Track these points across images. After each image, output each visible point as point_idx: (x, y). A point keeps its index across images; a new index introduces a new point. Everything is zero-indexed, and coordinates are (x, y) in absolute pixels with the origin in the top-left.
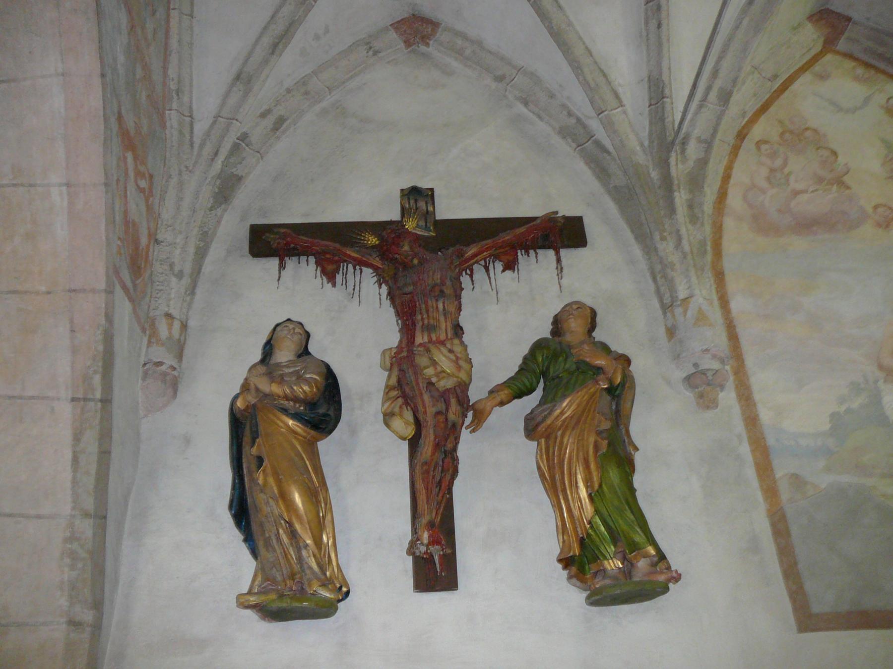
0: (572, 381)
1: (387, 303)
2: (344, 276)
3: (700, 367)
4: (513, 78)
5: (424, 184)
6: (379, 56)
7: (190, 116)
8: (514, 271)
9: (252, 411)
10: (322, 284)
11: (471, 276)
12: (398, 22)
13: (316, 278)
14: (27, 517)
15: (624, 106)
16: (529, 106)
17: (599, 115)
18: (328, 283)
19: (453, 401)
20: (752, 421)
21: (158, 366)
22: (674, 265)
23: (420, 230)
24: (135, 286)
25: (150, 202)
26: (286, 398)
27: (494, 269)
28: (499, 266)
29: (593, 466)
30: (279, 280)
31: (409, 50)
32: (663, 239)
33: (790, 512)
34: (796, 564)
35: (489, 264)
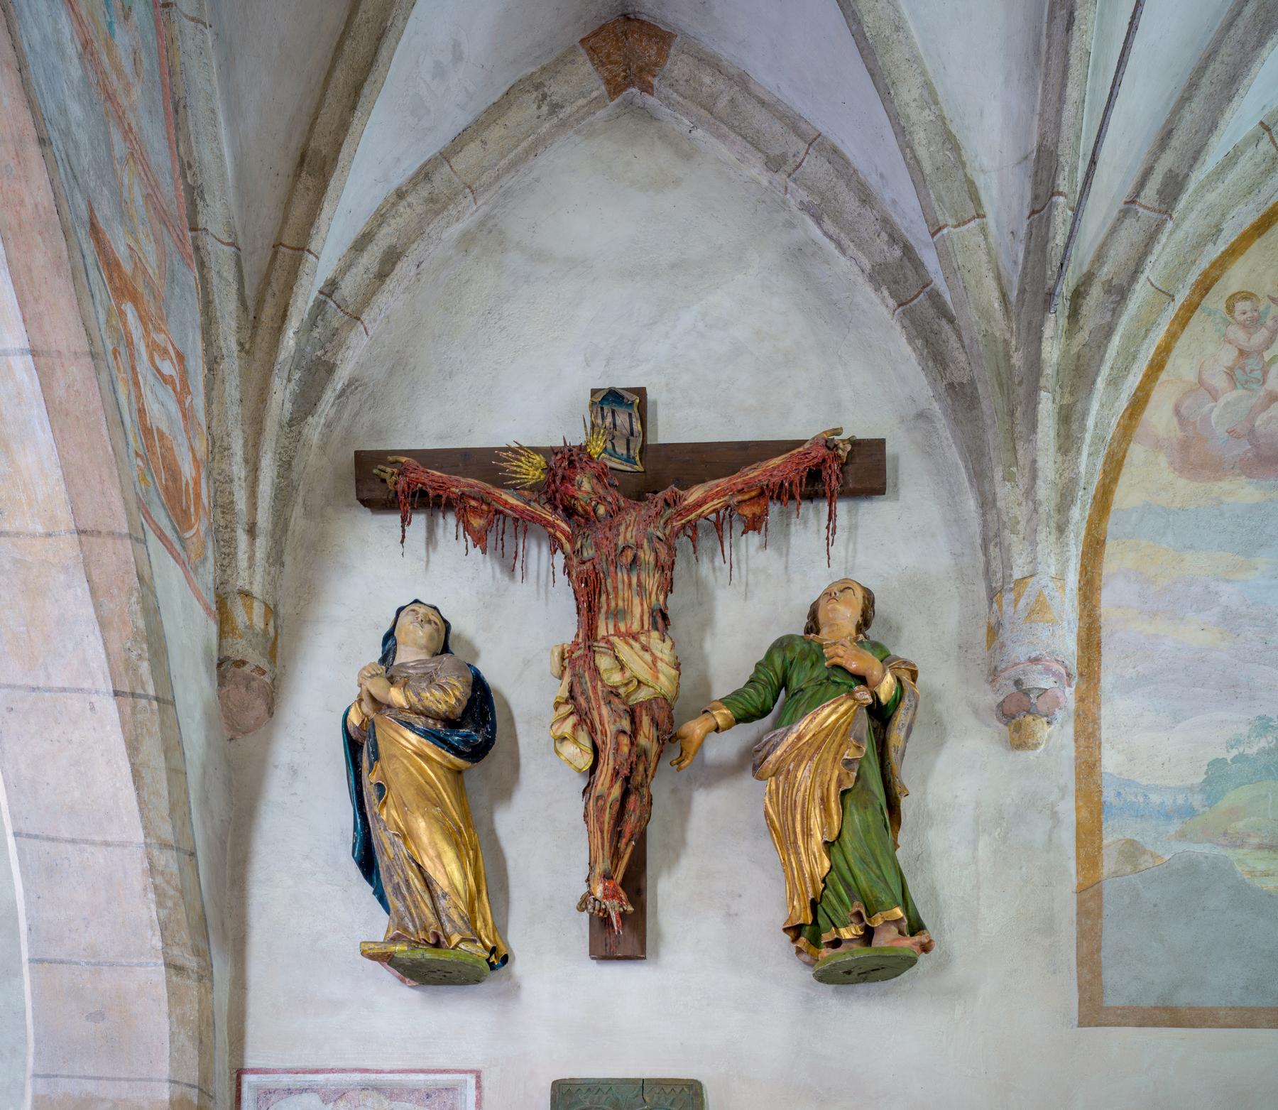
0: (819, 695)
1: (562, 578)
2: (500, 537)
3: (1025, 685)
5: (623, 381)
7: (232, 244)
8: (759, 533)
9: (368, 727)
10: (467, 548)
11: (693, 539)
14: (93, 843)
15: (984, 216)
17: (933, 235)
18: (475, 546)
19: (646, 721)
20: (1088, 768)
21: (239, 666)
22: (1018, 523)
23: (618, 461)
24: (182, 541)
25: (187, 405)
26: (412, 709)
27: (731, 528)
28: (738, 527)
30: (402, 542)
31: (617, 101)
32: (1009, 477)
33: (1108, 888)
34: (1099, 950)
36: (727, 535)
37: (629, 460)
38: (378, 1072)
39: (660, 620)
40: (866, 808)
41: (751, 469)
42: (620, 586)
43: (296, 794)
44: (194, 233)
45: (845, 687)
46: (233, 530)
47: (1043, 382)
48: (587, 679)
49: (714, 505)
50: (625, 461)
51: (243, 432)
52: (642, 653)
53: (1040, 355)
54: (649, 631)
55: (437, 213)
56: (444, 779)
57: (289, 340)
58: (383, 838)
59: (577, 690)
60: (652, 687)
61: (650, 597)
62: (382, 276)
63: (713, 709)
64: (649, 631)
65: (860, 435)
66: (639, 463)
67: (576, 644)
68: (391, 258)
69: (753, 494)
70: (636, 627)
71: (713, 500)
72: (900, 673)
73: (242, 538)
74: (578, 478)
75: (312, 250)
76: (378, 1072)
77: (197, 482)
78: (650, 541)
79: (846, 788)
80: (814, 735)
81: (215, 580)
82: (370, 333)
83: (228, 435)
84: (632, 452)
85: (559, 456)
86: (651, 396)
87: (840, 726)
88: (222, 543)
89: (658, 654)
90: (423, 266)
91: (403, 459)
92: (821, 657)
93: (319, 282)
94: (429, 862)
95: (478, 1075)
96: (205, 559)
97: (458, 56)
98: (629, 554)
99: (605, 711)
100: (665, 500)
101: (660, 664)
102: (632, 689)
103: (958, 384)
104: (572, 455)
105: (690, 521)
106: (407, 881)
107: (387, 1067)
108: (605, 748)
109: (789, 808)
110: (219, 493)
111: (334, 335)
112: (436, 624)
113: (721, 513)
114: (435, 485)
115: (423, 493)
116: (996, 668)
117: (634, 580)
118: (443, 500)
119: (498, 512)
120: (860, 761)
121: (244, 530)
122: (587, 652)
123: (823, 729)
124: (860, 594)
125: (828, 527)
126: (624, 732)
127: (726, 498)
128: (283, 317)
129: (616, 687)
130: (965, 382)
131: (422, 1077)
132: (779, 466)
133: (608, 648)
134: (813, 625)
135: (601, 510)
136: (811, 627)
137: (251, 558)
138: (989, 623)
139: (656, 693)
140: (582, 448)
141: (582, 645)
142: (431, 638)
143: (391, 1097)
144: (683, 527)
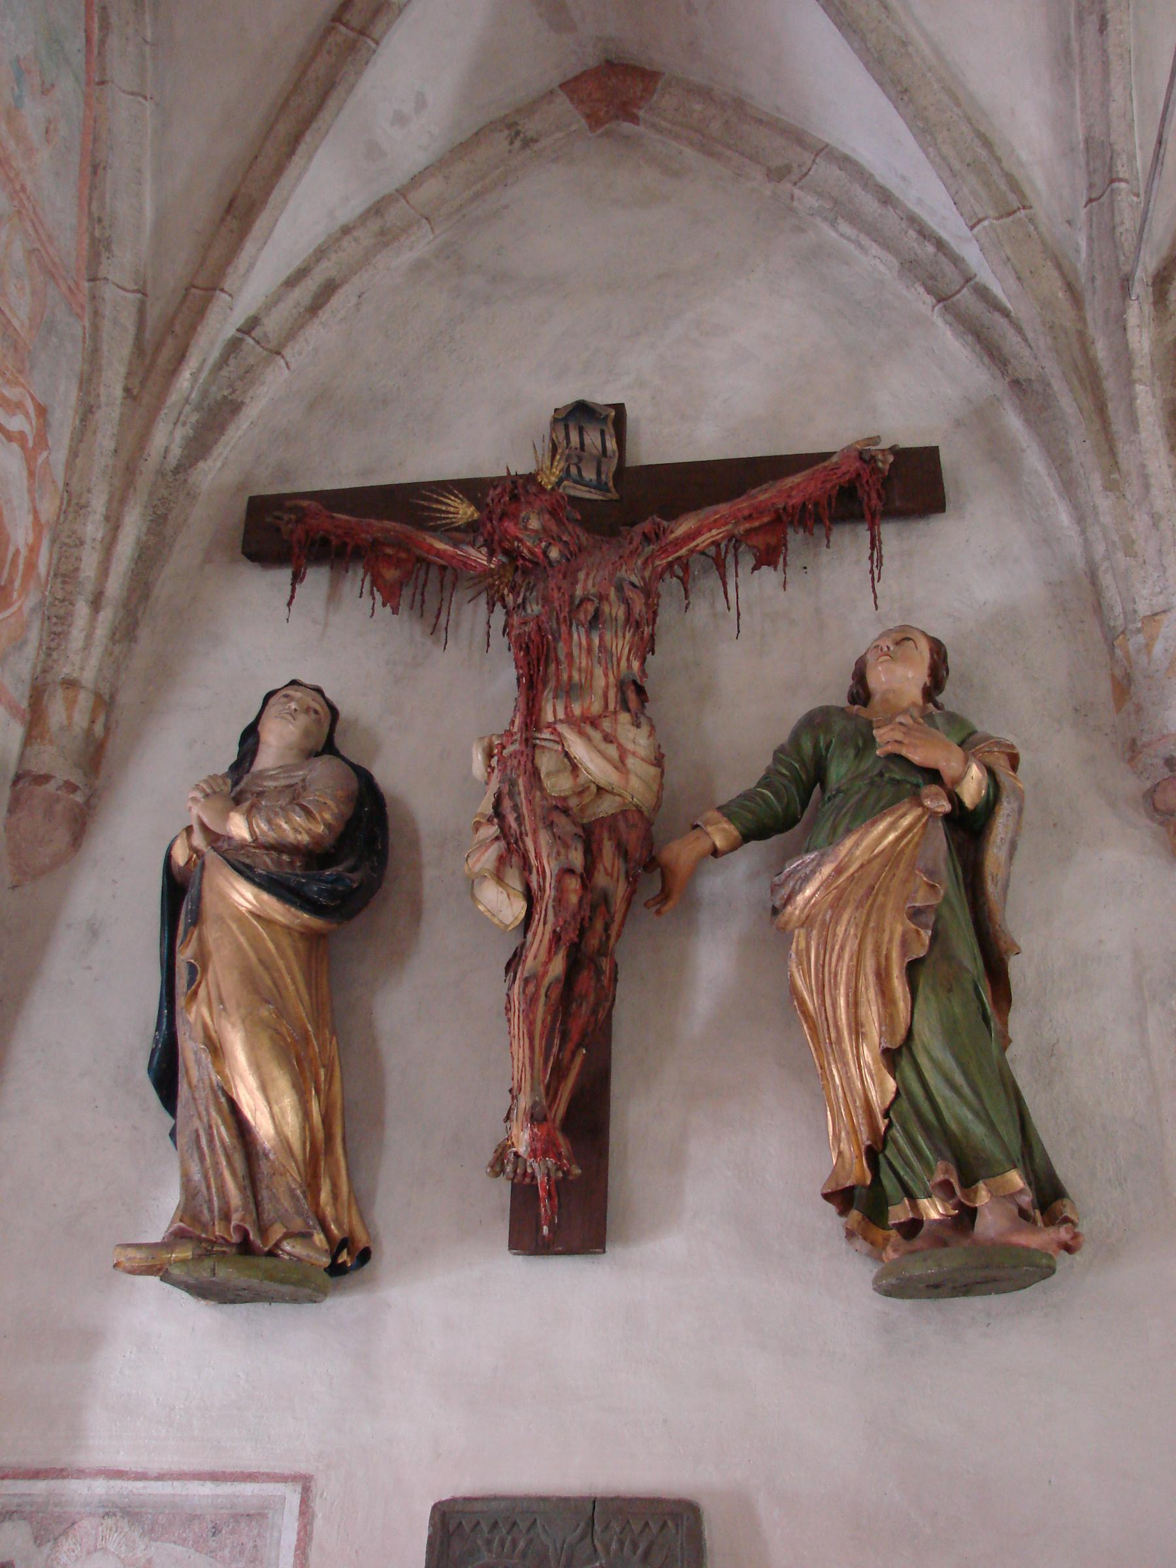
1: (500, 642)
4: (805, 170)
5: (602, 397)
6: (535, 148)
7: (138, 291)
8: (775, 569)
10: (373, 609)
12: (576, 79)
13: (361, 597)
16: (838, 224)
17: (972, 228)
18: (384, 605)
19: (608, 847)
23: (584, 488)
27: (737, 564)
28: (748, 560)
29: (815, 995)
30: (289, 604)
35: (726, 552)
36: (730, 572)
37: (600, 486)
38: (142, 1476)
39: (632, 696)
40: (950, 990)
41: (760, 491)
42: (576, 652)
43: (90, 968)
44: (91, 284)
45: (908, 786)
46: (72, 604)
47: (1136, 374)
48: (522, 788)
49: (712, 537)
50: (595, 488)
51: (111, 485)
52: (603, 746)
53: (1127, 345)
54: (615, 712)
55: (386, 245)
56: (290, 953)
57: (184, 380)
58: (190, 1048)
59: (507, 804)
60: (620, 795)
61: (618, 664)
62: (314, 308)
63: (707, 823)
64: (615, 712)
65: (906, 443)
66: (613, 489)
67: (509, 733)
68: (329, 289)
69: (766, 520)
70: (596, 708)
71: (710, 530)
72: (990, 759)
73: (82, 609)
74: (523, 514)
75: (226, 289)
76: (142, 1476)
77: (33, 549)
78: (620, 589)
79: (915, 957)
80: (862, 866)
81: (34, 668)
82: (292, 367)
83: (89, 491)
84: (603, 477)
85: (499, 490)
86: (631, 413)
87: (902, 850)
88: (54, 620)
89: (630, 746)
90: (364, 296)
91: (305, 503)
92: (870, 742)
93: (238, 318)
94: (248, 1097)
95: (305, 1483)
96: (25, 642)
97: (421, 103)
98: (591, 608)
99: (544, 837)
100: (644, 534)
101: (631, 761)
102: (589, 800)
103: (1025, 381)
104: (516, 487)
105: (679, 558)
106: (210, 1127)
107: (156, 1464)
108: (542, 898)
109: (827, 983)
110: (63, 559)
111: (247, 372)
112: (316, 712)
113: (723, 546)
114: (340, 532)
115: (325, 542)
116: (1134, 741)
117: (596, 641)
118: (349, 549)
119: (420, 560)
120: (936, 910)
121: (86, 601)
122: (523, 748)
123: (876, 856)
124: (924, 647)
125: (871, 558)
126: (571, 871)
127: (729, 527)
128: (180, 358)
129: (565, 799)
130: (1033, 378)
131: (207, 1489)
132: (798, 484)
133: (555, 741)
134: (861, 693)
135: (554, 554)
136: (858, 692)
137: (89, 637)
138: (1113, 677)
139: (624, 804)
140: (531, 478)
141: (518, 736)
142: (307, 733)
143: (152, 1530)
144: (670, 565)
